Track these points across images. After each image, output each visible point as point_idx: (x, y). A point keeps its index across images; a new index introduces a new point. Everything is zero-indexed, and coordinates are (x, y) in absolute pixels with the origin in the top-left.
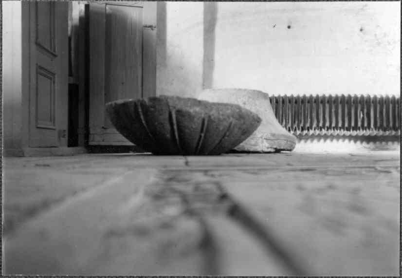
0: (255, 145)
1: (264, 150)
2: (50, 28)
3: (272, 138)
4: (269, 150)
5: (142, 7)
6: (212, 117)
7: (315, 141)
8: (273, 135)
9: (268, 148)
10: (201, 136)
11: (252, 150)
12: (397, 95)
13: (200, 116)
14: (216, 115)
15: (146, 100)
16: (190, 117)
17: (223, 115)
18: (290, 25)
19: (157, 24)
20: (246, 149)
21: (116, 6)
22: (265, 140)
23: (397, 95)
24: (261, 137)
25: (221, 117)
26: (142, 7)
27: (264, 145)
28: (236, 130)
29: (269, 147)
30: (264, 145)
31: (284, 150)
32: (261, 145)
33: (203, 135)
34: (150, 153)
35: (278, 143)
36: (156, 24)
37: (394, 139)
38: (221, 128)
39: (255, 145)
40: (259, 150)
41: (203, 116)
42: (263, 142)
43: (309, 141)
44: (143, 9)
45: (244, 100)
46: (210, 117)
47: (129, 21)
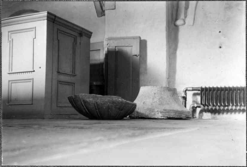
0: (154, 115)
1: (159, 118)
2: (73, 65)
3: (164, 111)
4: (162, 118)
5: (132, 46)
6: (98, 103)
7: (237, 113)
8: (165, 110)
9: (161, 117)
10: (97, 111)
11: (152, 117)
12: (244, 85)
13: (92, 102)
14: (100, 102)
15: (73, 96)
16: (89, 103)
17: (103, 102)
18: (220, 46)
19: (140, 53)
20: (149, 117)
21: (122, 47)
22: (159, 113)
23: (244, 85)
24: (158, 111)
25: (102, 103)
26: (132, 46)
27: (159, 115)
28: (114, 108)
29: (162, 116)
30: (159, 115)
31: (166, 119)
32: (157, 115)
33: (97, 110)
34: (87, 118)
35: (169, 114)
36: (139, 54)
37: (243, 111)
38: (104, 108)
39: (154, 115)
40: (156, 117)
41: (94, 102)
42: (158, 114)
43: (233, 113)
44: (133, 47)
45: (155, 92)
46: (97, 103)
47: (129, 53)
